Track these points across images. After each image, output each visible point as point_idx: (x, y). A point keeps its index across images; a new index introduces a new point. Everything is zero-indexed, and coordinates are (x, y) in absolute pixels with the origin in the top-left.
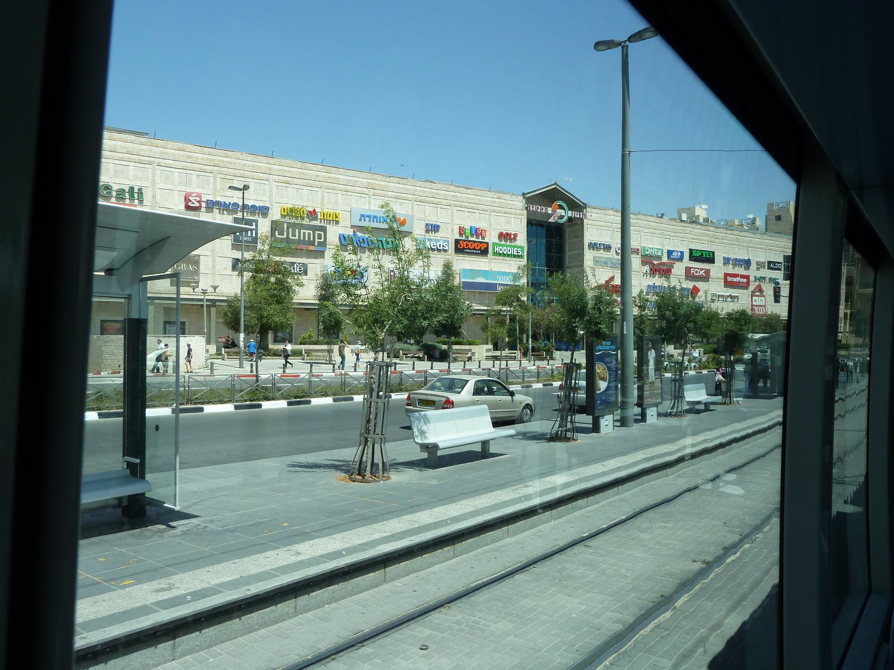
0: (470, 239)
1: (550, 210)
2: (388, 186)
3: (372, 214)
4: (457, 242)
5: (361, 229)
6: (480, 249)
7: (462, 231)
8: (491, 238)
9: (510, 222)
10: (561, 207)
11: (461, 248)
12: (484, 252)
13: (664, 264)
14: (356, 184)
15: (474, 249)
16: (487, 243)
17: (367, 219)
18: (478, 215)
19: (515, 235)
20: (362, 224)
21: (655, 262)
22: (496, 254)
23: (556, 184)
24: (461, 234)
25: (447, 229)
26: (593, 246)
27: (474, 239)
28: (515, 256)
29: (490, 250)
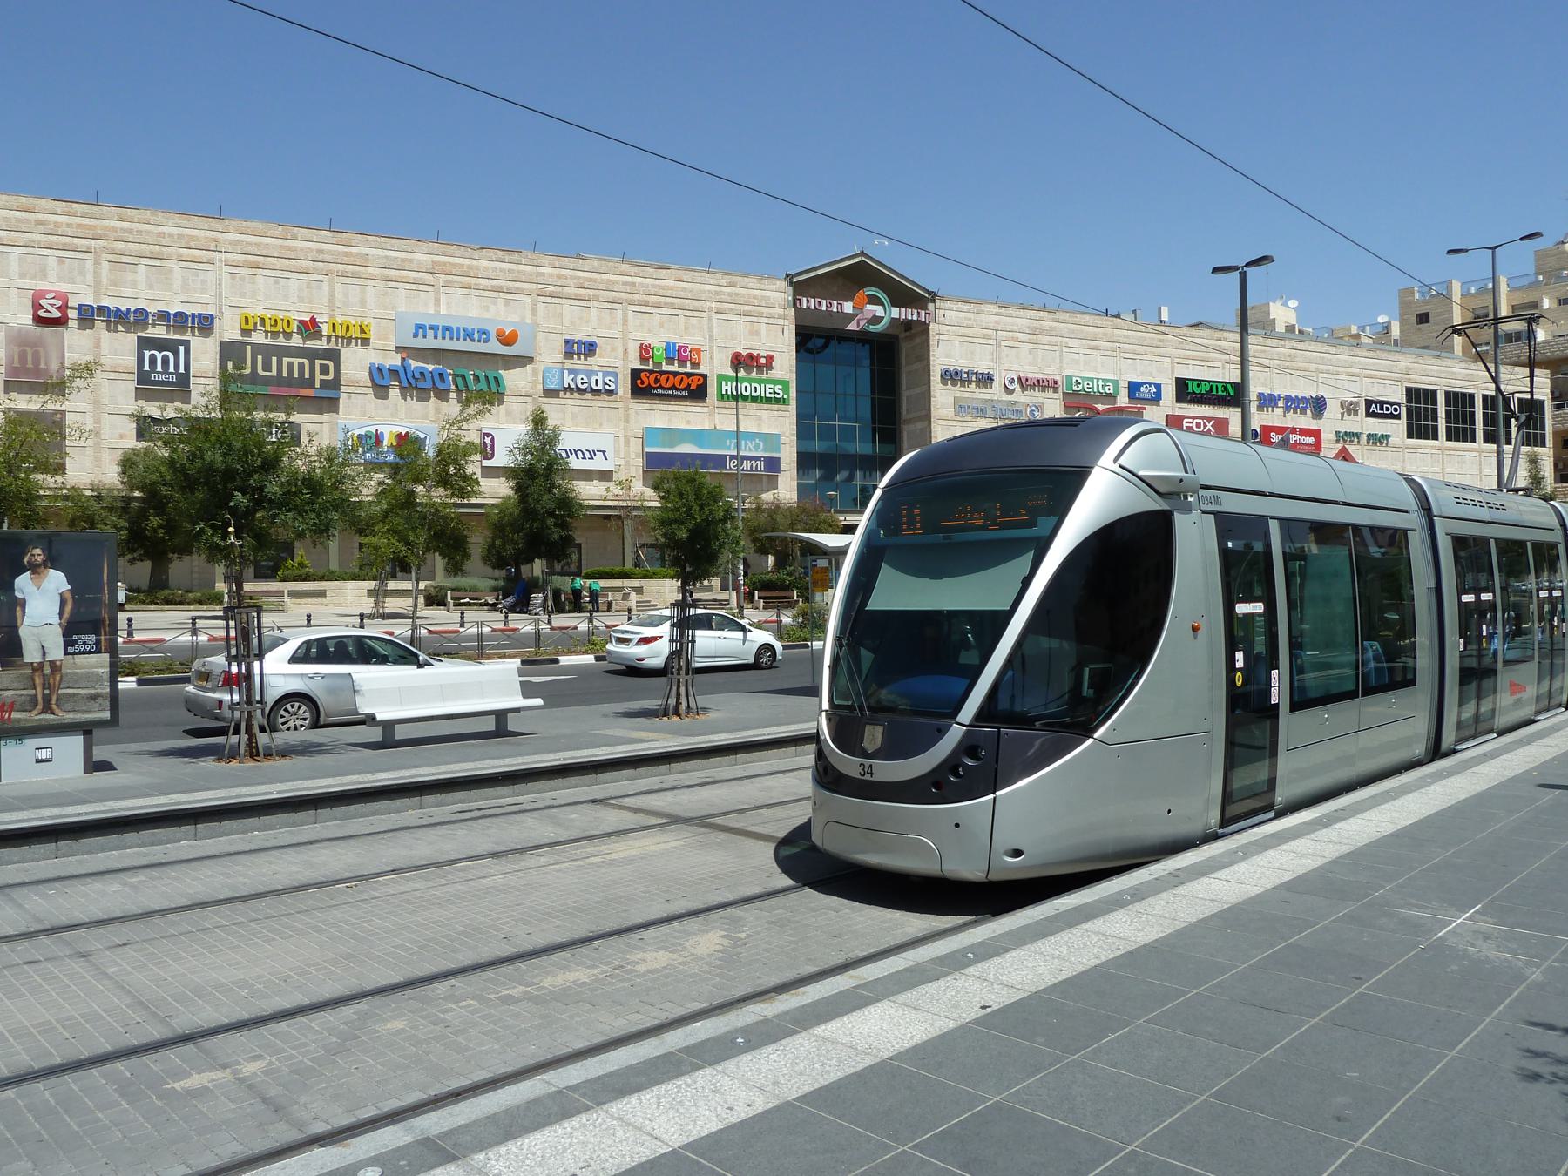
0: (665, 368)
1: (848, 307)
2: (477, 268)
3: (441, 324)
4: (635, 374)
5: (420, 353)
6: (688, 388)
7: (645, 352)
8: (715, 365)
9: (757, 333)
10: (874, 300)
11: (645, 386)
12: (697, 393)
13: (1121, 410)
14: (447, 270)
15: (674, 387)
16: (705, 376)
17: (430, 333)
18: (682, 319)
19: (770, 358)
20: (420, 343)
21: (1100, 407)
22: (723, 397)
23: (862, 254)
24: (644, 360)
25: (614, 349)
26: (951, 377)
27: (675, 368)
28: (769, 401)
29: (712, 390)
